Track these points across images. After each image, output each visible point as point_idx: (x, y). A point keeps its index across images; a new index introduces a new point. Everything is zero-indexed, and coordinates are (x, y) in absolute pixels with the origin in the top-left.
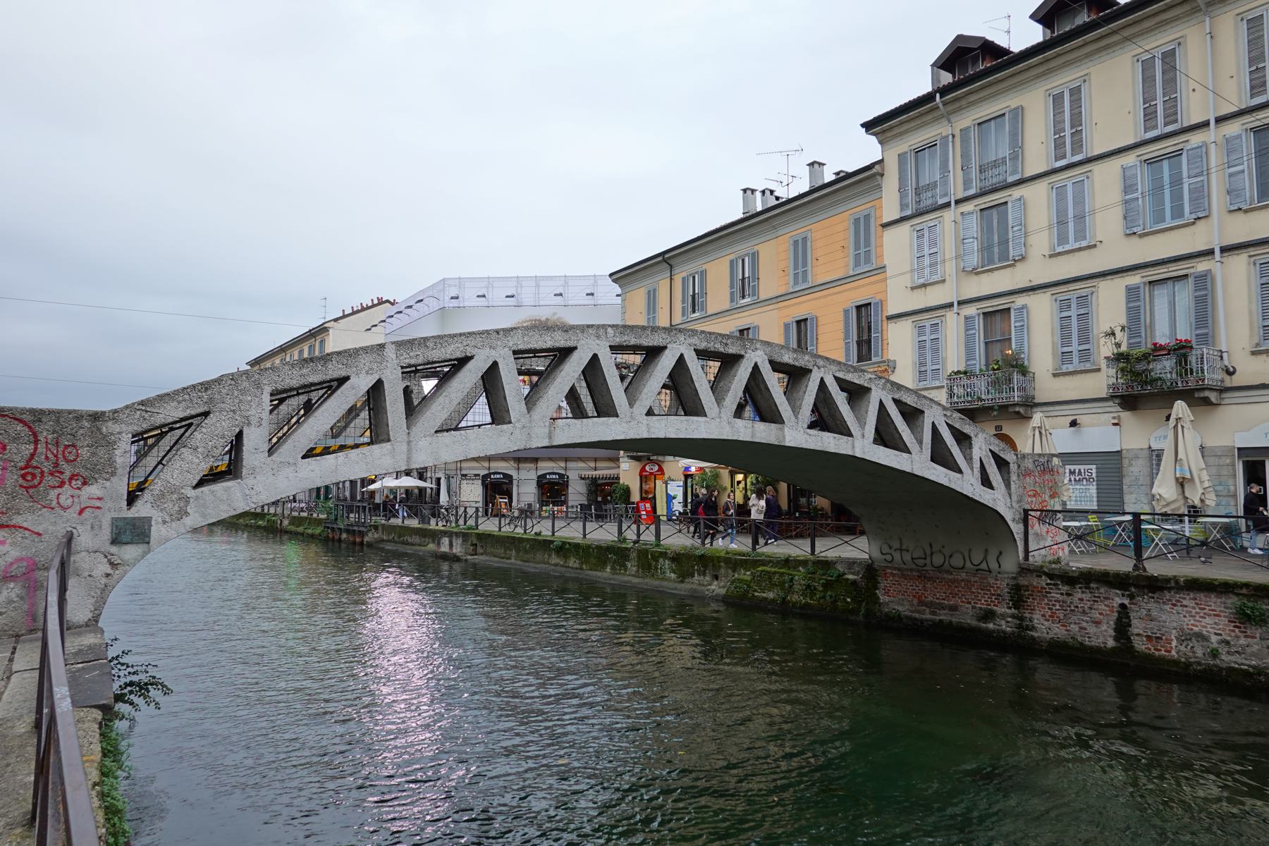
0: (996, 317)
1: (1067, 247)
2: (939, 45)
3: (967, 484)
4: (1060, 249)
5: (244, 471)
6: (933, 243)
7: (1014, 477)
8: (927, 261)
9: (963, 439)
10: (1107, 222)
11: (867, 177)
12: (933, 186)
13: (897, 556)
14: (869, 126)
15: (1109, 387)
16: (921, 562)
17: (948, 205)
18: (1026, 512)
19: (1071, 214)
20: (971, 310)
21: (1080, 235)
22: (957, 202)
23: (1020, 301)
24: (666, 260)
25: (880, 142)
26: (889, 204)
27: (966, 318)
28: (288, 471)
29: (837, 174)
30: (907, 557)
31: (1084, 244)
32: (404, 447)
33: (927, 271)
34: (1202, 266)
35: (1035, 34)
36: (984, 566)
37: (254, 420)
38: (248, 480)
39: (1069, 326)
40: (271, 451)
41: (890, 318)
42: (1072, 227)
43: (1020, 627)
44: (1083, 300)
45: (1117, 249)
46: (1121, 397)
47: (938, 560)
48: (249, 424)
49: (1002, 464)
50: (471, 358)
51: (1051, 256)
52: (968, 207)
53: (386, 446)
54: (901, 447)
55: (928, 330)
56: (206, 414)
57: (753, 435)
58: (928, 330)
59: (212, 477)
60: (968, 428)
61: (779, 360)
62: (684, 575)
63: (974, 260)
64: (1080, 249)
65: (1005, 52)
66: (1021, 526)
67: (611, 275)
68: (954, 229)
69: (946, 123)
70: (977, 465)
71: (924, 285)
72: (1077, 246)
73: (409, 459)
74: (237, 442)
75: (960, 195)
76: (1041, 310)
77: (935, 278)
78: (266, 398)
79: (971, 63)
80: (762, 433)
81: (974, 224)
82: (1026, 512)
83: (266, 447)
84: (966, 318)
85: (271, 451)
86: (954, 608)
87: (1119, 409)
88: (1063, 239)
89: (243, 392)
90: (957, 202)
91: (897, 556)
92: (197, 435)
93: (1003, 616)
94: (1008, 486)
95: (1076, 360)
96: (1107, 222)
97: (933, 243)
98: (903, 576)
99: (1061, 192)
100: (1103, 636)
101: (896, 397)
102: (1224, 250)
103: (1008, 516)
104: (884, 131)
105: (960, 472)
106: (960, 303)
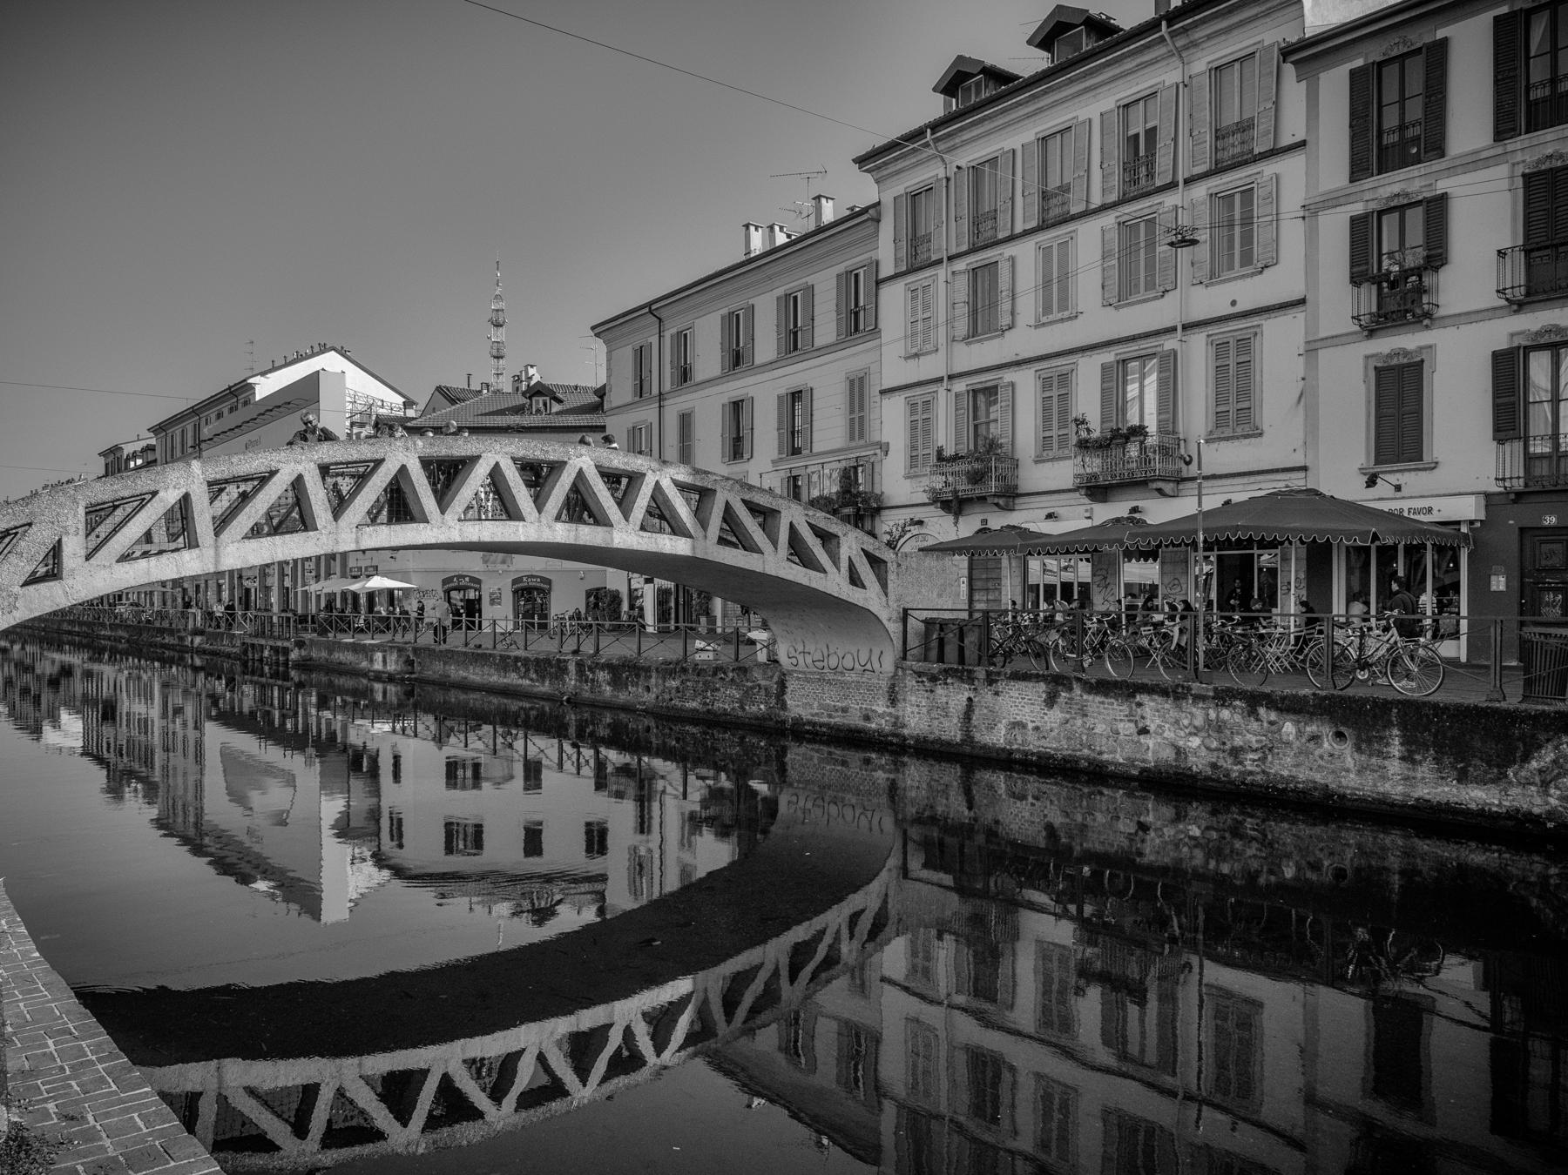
0: (984, 394)
1: (1051, 318)
2: (939, 68)
3: (834, 583)
4: (1044, 320)
5: (65, 573)
6: (926, 307)
7: (891, 577)
8: (920, 326)
9: (826, 538)
10: (1088, 285)
11: (863, 218)
12: (1065, 189)
13: (801, 658)
14: (861, 161)
15: (1076, 476)
16: (820, 664)
17: (940, 261)
18: (905, 611)
19: (1055, 275)
20: (960, 386)
21: (1063, 306)
22: (950, 258)
23: (1008, 376)
24: (652, 309)
25: (877, 182)
26: (886, 251)
27: (957, 395)
28: (104, 573)
29: (852, 209)
30: (809, 660)
31: (1066, 314)
32: (212, 552)
33: (920, 339)
34: (1169, 343)
35: (1039, 61)
36: (869, 667)
37: (72, 530)
38: (68, 581)
39: (1050, 408)
40: (88, 558)
41: (882, 392)
42: (1056, 297)
43: (895, 724)
44: (1244, 344)
45: (1097, 319)
46: (1088, 488)
47: (833, 662)
48: (67, 533)
49: (875, 562)
50: (277, 471)
51: (1036, 327)
52: (960, 265)
53: (195, 552)
54: (749, 546)
55: (920, 408)
56: (30, 525)
57: (576, 537)
58: (920, 408)
59: (33, 580)
60: (835, 527)
61: (607, 464)
62: (616, 682)
63: (962, 327)
64: (1062, 320)
65: (1014, 78)
66: (900, 626)
67: (593, 328)
68: (946, 287)
69: (1178, 63)
70: (844, 565)
71: (916, 355)
72: (1060, 316)
73: (217, 562)
74: (56, 551)
75: (953, 251)
76: (1026, 384)
77: (929, 347)
78: (81, 511)
79: (974, 88)
80: (587, 535)
81: (962, 283)
82: (905, 611)
83: (83, 553)
84: (957, 395)
85: (88, 558)
86: (845, 710)
87: (1087, 501)
88: (1047, 309)
89: (61, 505)
90: (950, 258)
91: (801, 658)
92: (23, 544)
93: (881, 716)
94: (884, 585)
95: (1055, 446)
96: (1088, 285)
97: (926, 307)
98: (807, 680)
99: (1047, 252)
100: (951, 730)
101: (747, 497)
102: (1185, 327)
103: (883, 616)
104: (878, 168)
105: (825, 571)
106: (951, 377)
